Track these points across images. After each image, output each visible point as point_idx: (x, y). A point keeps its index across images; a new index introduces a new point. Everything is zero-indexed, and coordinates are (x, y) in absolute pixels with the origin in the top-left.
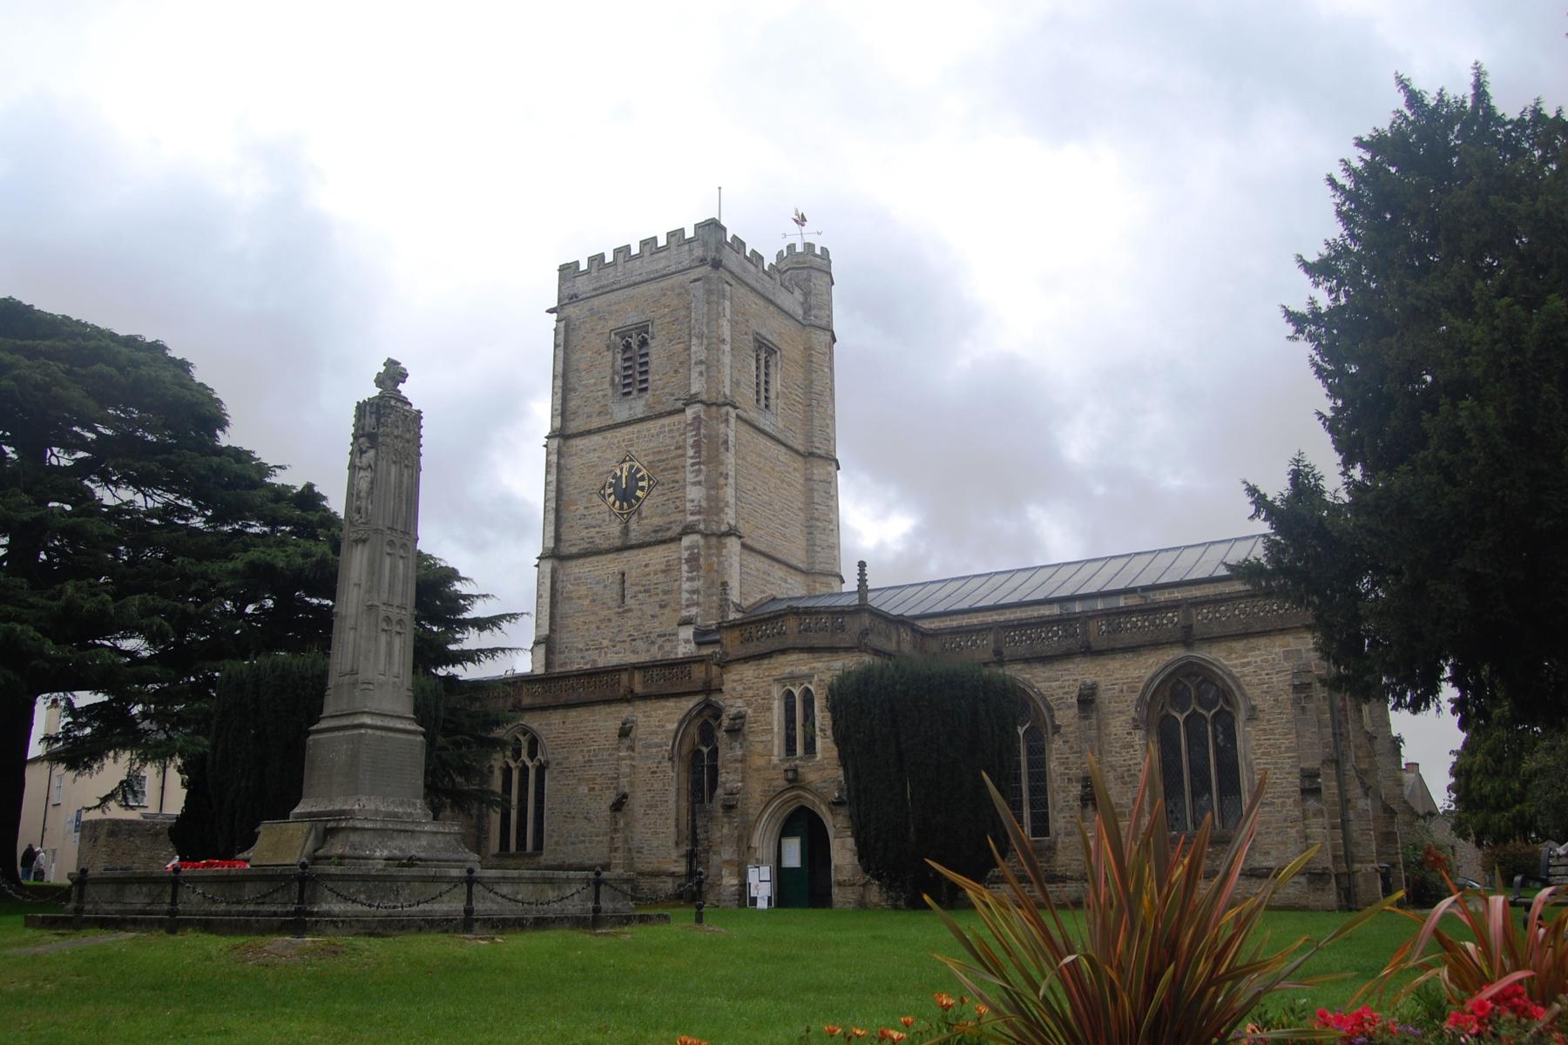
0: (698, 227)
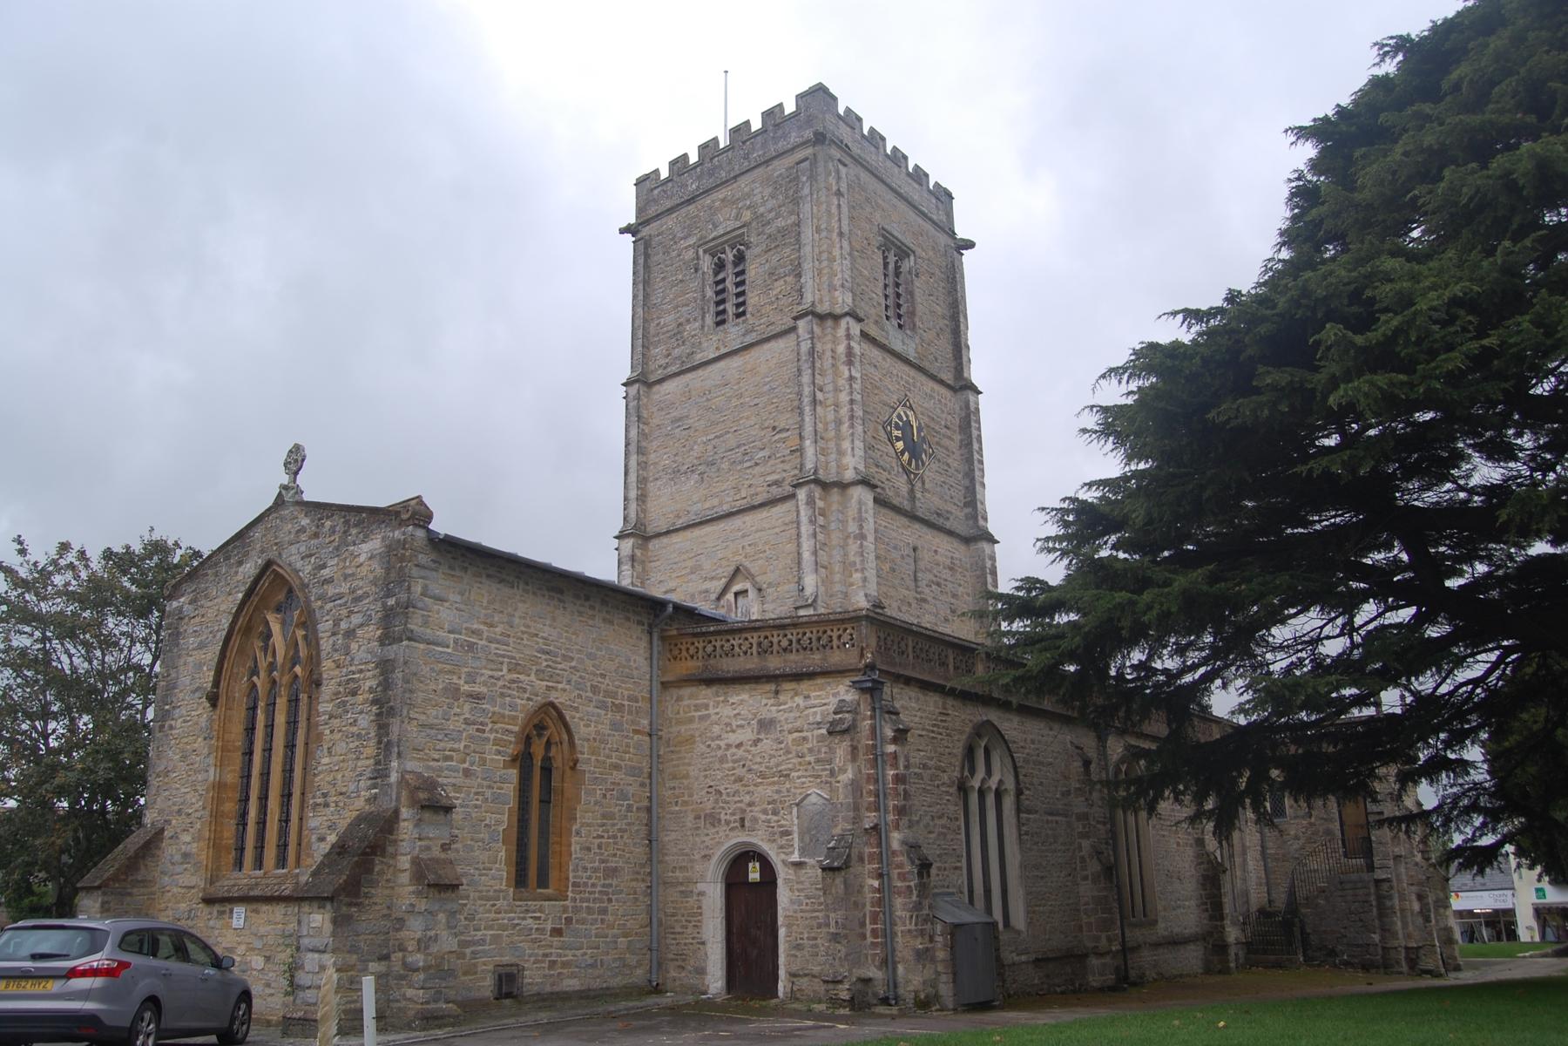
0: (800, 97)
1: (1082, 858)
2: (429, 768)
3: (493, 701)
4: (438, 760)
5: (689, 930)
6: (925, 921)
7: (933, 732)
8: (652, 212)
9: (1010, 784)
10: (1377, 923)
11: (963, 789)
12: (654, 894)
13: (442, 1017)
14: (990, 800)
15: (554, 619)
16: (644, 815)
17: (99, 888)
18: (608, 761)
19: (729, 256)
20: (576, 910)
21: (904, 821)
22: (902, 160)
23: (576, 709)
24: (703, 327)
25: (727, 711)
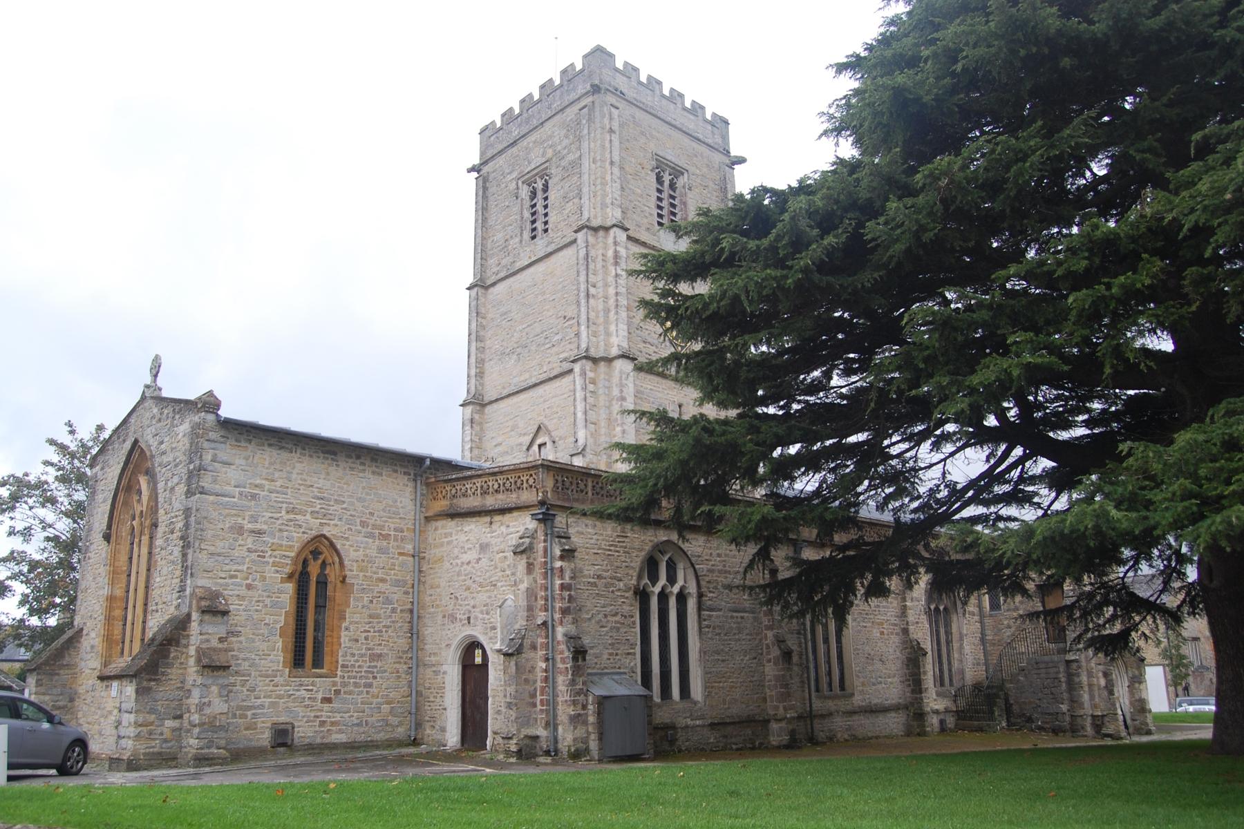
1: (767, 645)
2: (217, 584)
3: (272, 535)
4: (224, 578)
5: (438, 700)
6: (579, 693)
7: (610, 550)
8: (489, 154)
9: (692, 589)
10: (1066, 695)
11: (642, 596)
12: (414, 673)
13: (212, 759)
14: (672, 602)
15: (328, 474)
16: (407, 616)
17: (34, 670)
18: (375, 576)
19: (539, 185)
20: (345, 685)
21: (569, 618)
22: (678, 98)
23: (347, 539)
24: (521, 241)
25: (463, 538)
